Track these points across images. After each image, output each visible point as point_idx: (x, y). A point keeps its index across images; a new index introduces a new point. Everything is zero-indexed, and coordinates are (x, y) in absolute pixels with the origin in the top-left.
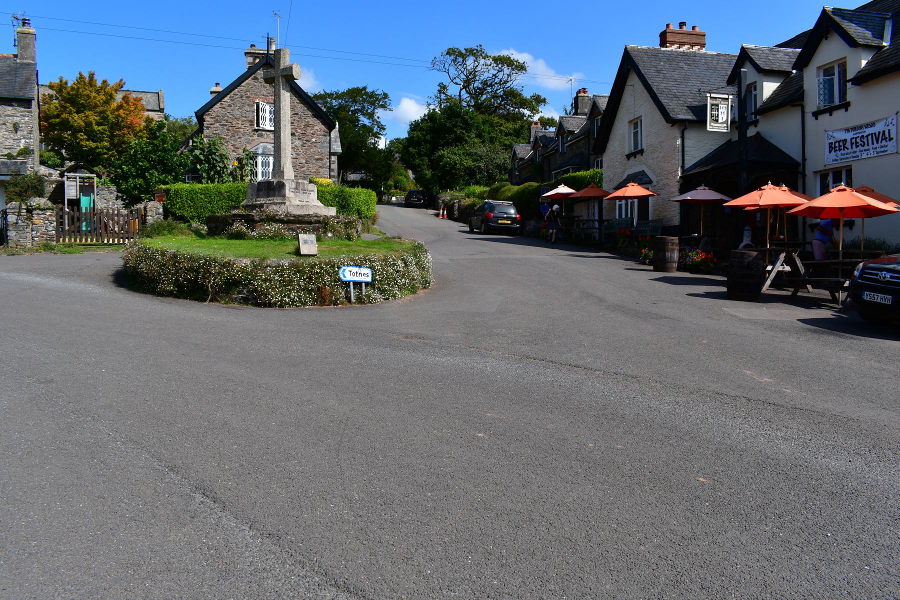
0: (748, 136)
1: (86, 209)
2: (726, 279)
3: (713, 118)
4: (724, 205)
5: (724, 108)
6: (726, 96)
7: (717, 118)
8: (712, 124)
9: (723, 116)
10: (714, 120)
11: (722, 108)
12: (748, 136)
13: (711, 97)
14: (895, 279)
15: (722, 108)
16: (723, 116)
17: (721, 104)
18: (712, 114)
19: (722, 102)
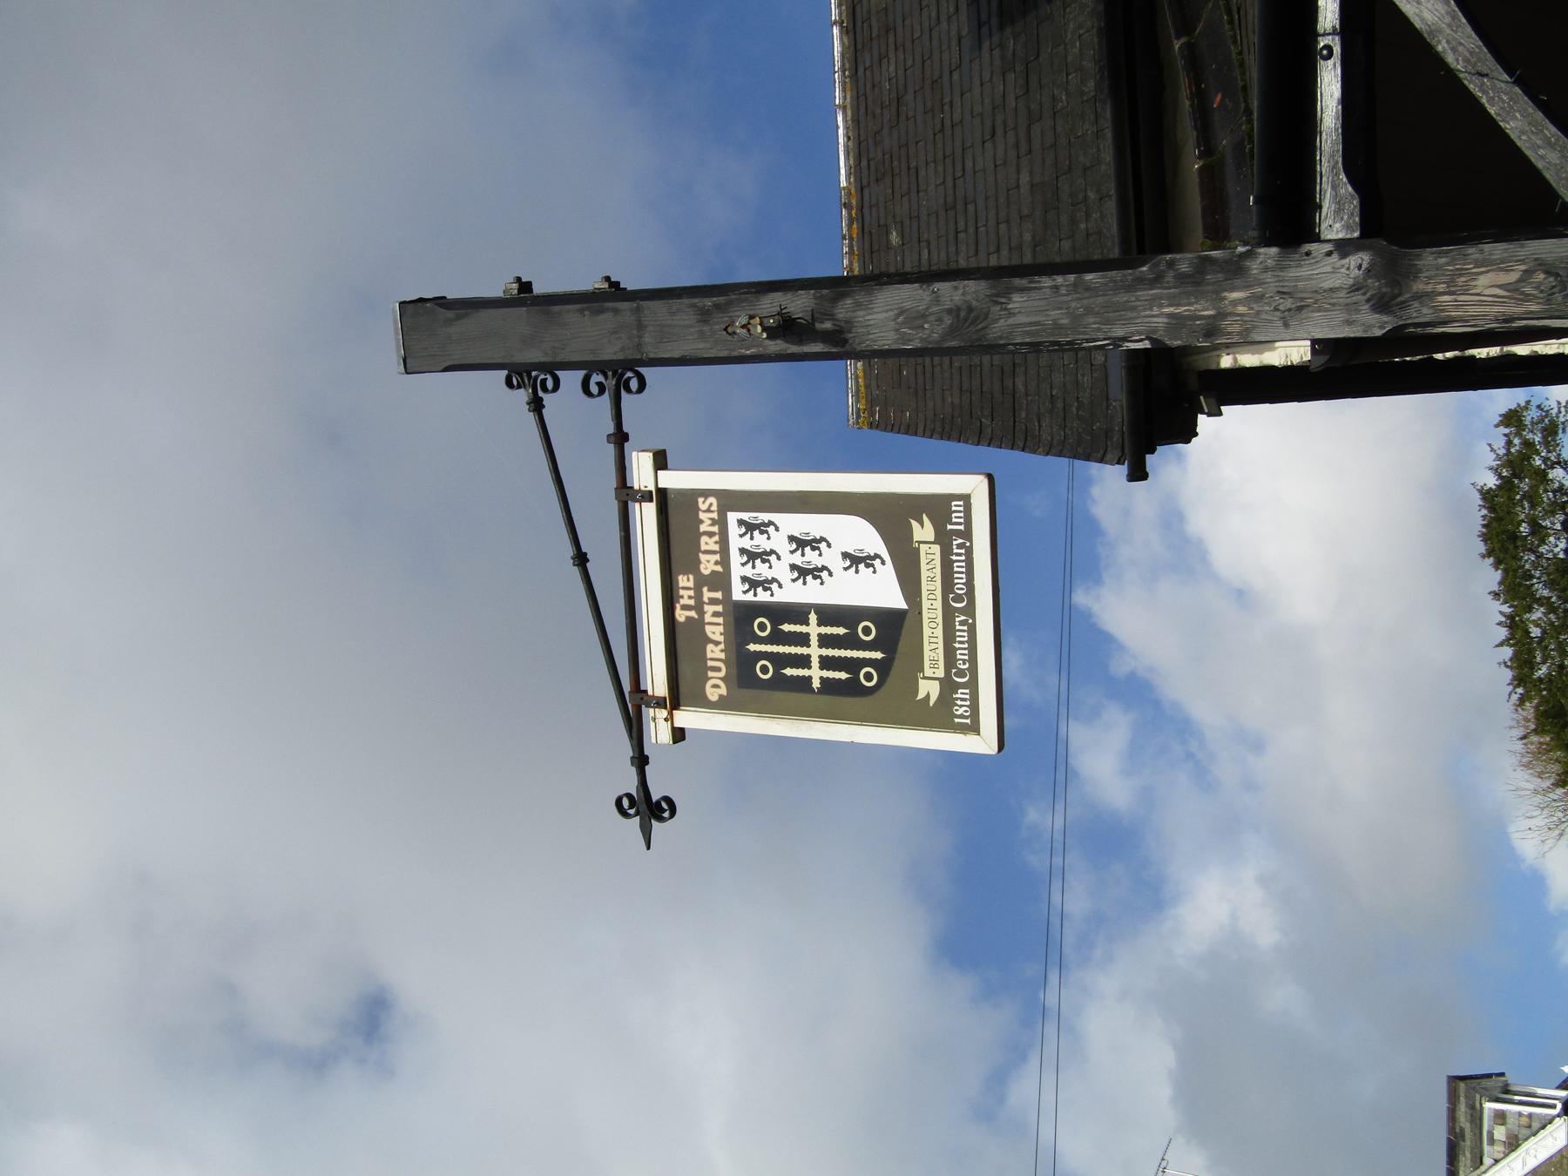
0: (1222, 407)
1: (1298, 279)
2: (1201, 397)
3: (868, 678)
4: (931, 705)
5: (760, 542)
6: (646, 517)
7: (868, 631)
8: (929, 689)
9: (831, 558)
10: (883, 667)
11: (761, 570)
12: (1222, 407)
13: (675, 701)
14: (1536, 359)
15: (761, 570)
16: (831, 558)
17: (721, 581)
18: (828, 686)
19: (708, 565)
